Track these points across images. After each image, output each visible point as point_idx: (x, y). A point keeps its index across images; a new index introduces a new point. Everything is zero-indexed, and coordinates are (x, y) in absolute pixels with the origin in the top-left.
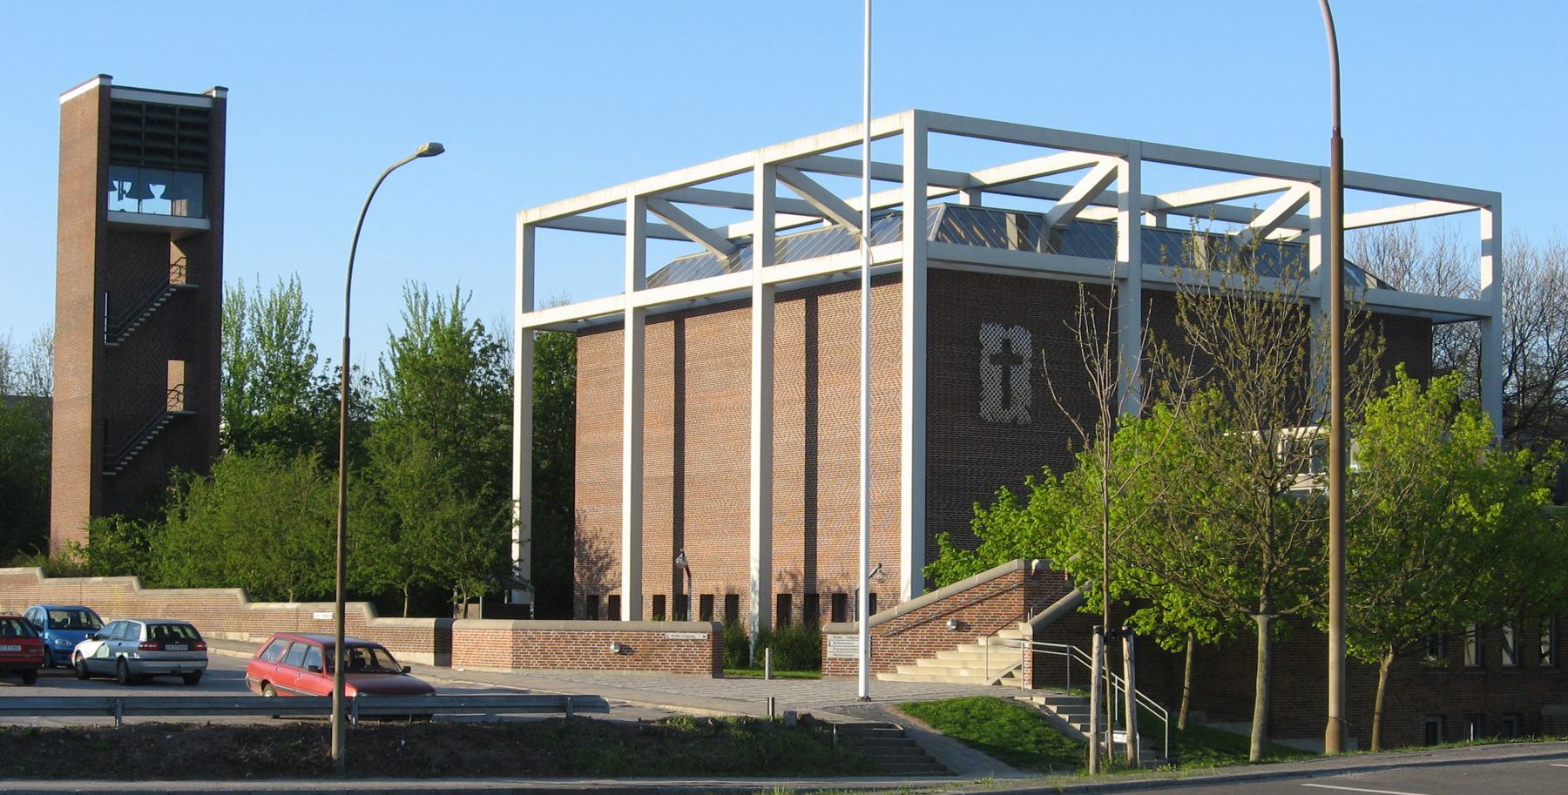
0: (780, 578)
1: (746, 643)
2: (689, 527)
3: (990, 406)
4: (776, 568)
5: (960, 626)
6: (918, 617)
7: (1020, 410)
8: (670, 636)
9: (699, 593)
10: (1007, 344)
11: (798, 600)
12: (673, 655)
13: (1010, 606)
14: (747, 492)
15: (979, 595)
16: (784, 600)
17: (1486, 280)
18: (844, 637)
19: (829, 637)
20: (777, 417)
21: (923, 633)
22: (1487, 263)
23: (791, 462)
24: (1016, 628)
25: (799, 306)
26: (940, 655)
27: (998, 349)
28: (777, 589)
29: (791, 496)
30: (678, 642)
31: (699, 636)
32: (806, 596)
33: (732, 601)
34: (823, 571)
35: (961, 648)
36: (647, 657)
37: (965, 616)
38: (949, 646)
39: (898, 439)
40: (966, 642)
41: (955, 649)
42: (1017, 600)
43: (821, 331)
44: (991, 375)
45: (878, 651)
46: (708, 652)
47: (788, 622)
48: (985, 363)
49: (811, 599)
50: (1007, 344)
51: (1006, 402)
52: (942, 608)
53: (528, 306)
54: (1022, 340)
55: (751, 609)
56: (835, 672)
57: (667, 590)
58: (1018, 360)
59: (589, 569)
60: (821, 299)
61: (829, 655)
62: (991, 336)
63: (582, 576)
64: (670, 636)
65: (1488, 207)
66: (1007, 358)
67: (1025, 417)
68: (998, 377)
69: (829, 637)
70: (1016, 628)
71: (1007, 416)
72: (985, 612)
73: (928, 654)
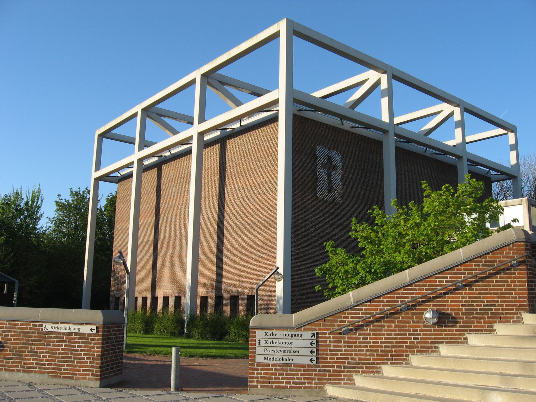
0: (205, 285)
1: (183, 322)
2: (159, 264)
3: (322, 191)
4: (201, 283)
5: (443, 319)
6: (383, 307)
7: (336, 195)
8: (48, 327)
9: (162, 296)
10: (329, 158)
11: (212, 298)
12: (52, 353)
13: (509, 292)
14: (186, 237)
15: (468, 276)
16: (204, 299)
17: (513, 161)
18: (280, 334)
19: (260, 334)
20: (203, 205)
21: (389, 329)
22: (513, 154)
23: (210, 226)
24: (519, 321)
25: (217, 148)
26: (415, 359)
27: (325, 161)
28: (201, 292)
29: (209, 245)
30: (59, 337)
31: (85, 329)
32: (216, 297)
33: (178, 300)
34: (227, 281)
35: (444, 350)
36: (19, 355)
37: (449, 305)
38: (428, 348)
39: (274, 207)
40: (451, 341)
41: (435, 350)
42: (518, 282)
43: (228, 157)
44: (322, 174)
45: (327, 354)
46: (96, 350)
47: (206, 311)
48: (319, 167)
49: (219, 298)
50: (329, 158)
51: (330, 190)
52: (417, 293)
53: (98, 168)
54: (337, 159)
55: (187, 300)
56: (267, 382)
57: (148, 294)
58: (335, 168)
59: (118, 284)
60: (228, 142)
61: (259, 359)
62: (322, 153)
63: (115, 287)
64: (48, 327)
65: (512, 132)
66: (330, 166)
67: (339, 199)
68: (326, 176)
69: (260, 334)
70: (519, 321)
71: (329, 197)
72: (475, 299)
73: (398, 358)
